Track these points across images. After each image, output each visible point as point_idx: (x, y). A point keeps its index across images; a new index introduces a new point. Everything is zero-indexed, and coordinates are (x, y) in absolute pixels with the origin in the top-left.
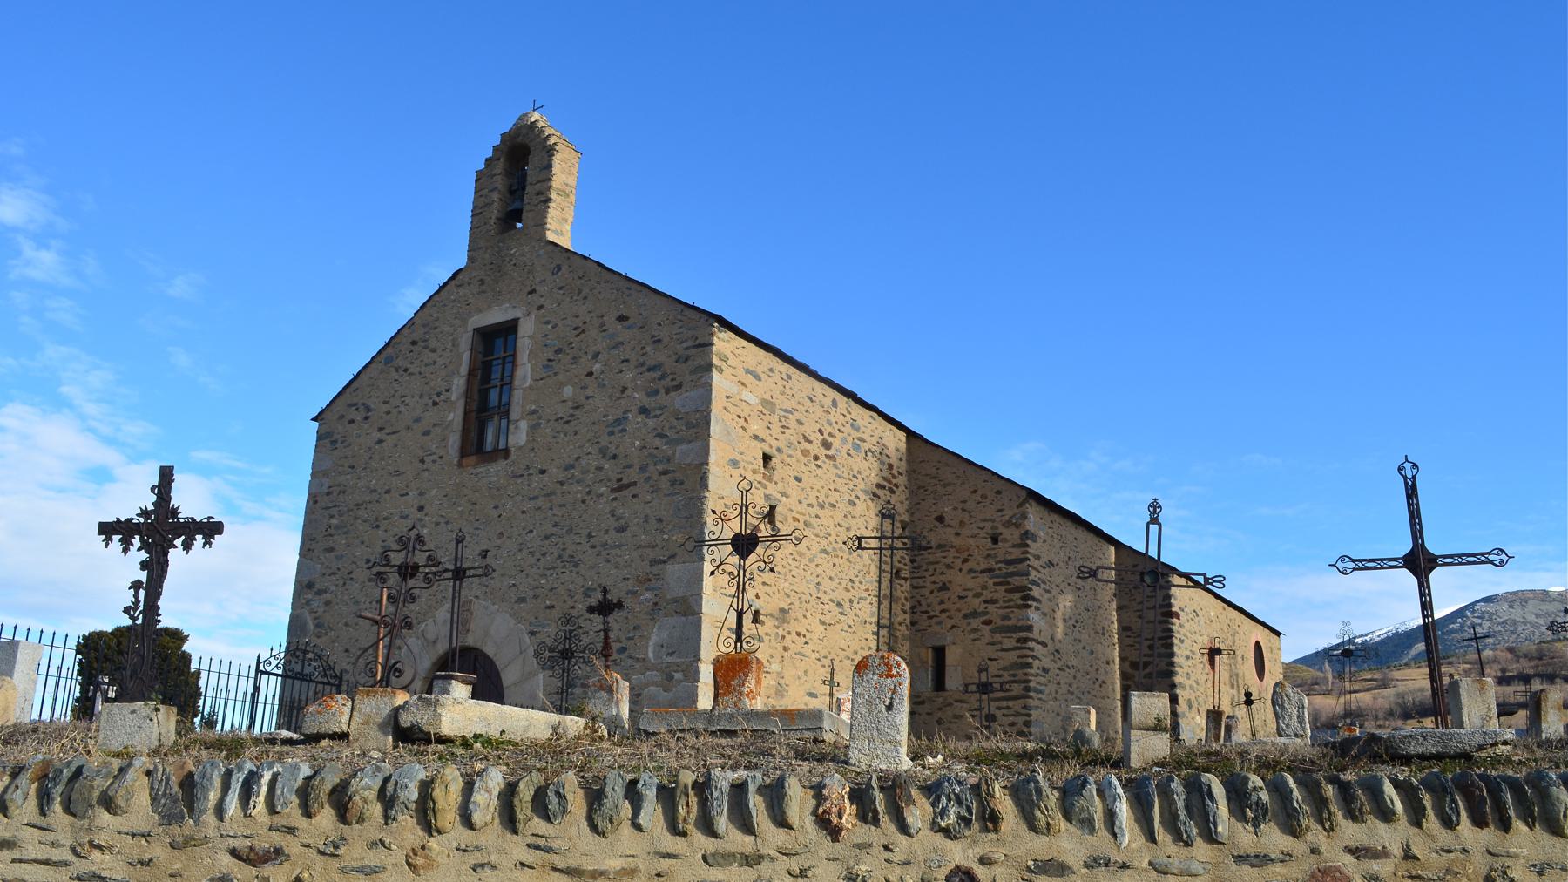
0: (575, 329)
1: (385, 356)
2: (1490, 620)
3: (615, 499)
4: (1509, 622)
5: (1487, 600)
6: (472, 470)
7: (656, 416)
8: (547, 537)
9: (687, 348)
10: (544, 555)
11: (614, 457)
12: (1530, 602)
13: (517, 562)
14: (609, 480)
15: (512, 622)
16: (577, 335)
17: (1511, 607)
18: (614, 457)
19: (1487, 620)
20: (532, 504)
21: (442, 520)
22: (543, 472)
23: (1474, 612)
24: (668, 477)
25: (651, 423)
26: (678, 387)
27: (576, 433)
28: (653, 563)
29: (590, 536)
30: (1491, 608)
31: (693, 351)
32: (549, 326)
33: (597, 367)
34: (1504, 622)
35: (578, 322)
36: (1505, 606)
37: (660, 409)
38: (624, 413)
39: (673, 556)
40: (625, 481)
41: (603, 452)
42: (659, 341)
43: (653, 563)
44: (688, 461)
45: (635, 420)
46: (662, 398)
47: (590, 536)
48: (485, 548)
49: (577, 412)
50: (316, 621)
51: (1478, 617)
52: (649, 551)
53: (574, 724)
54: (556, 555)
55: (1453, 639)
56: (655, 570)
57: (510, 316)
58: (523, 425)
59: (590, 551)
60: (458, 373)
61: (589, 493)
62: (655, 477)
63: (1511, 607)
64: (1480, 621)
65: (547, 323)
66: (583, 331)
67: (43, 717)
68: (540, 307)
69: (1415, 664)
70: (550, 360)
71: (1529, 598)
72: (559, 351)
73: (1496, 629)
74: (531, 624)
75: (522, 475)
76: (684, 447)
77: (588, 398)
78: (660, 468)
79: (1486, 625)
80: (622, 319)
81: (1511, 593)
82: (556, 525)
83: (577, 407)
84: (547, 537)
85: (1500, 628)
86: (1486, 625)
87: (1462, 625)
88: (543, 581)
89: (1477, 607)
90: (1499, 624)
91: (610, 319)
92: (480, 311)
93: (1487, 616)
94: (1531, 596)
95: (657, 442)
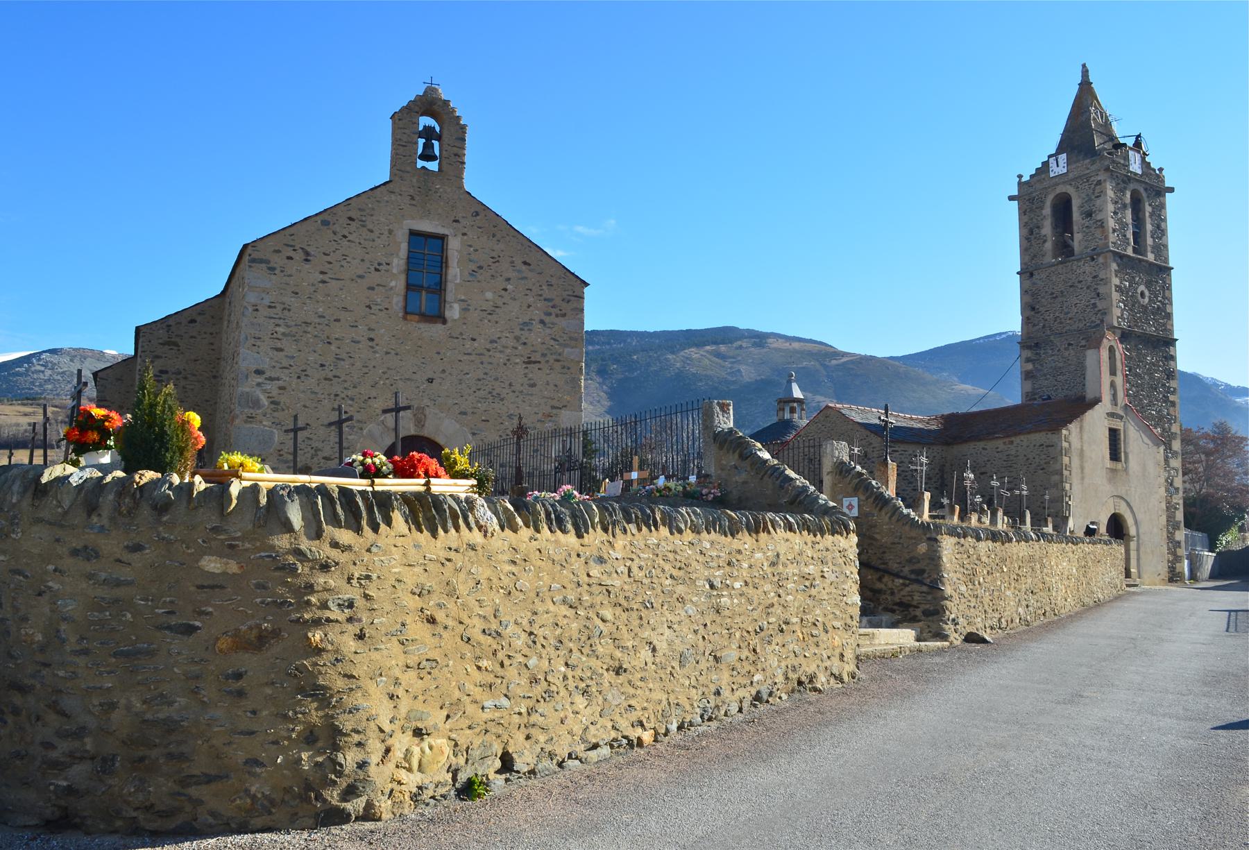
0: (492, 258)
1: (325, 218)
2: (52, 369)
3: (527, 368)
4: (67, 373)
5: (53, 352)
6: (415, 324)
7: (549, 327)
8: (479, 380)
9: (569, 295)
10: (479, 390)
11: (525, 344)
12: (89, 359)
13: (458, 390)
14: (522, 356)
15: (458, 426)
16: (494, 263)
17: (71, 360)
18: (525, 344)
19: (50, 369)
20: (466, 357)
21: (393, 352)
22: (474, 340)
23: (39, 360)
24: (560, 363)
25: (548, 331)
26: (564, 315)
27: (497, 322)
28: (553, 407)
29: (510, 385)
30: (55, 359)
31: (573, 298)
32: (472, 249)
33: (509, 287)
34: (63, 373)
35: (494, 254)
36: (66, 359)
37: (552, 324)
38: (530, 320)
39: (565, 406)
40: (533, 359)
41: (517, 338)
42: (551, 285)
43: (553, 407)
44: (572, 357)
45: (537, 327)
46: (553, 318)
47: (510, 385)
48: (431, 377)
49: (497, 310)
50: (271, 400)
51: (42, 365)
52: (550, 400)
53: (1050, 519)
54: (487, 390)
55: (17, 380)
56: (555, 411)
57: (441, 231)
58: (456, 306)
59: (511, 394)
60: (397, 255)
61: (508, 360)
62: (552, 361)
63: (71, 360)
64: (43, 369)
65: (470, 246)
66: (498, 261)
67: (35, 462)
68: (464, 234)
69: (8, 401)
70: (473, 271)
71: (89, 356)
72: (480, 268)
73: (56, 377)
74: (471, 429)
75: (457, 338)
76: (569, 349)
77: (504, 304)
78: (554, 357)
79: (48, 373)
80: (525, 263)
81: (74, 349)
82: (486, 374)
83: (497, 307)
84: (479, 380)
85: (59, 377)
86: (48, 373)
87: (27, 370)
88: (479, 405)
89: (43, 356)
90: (59, 373)
91: (518, 261)
92: (413, 218)
93: (50, 365)
94: (90, 354)
95: (552, 342)
